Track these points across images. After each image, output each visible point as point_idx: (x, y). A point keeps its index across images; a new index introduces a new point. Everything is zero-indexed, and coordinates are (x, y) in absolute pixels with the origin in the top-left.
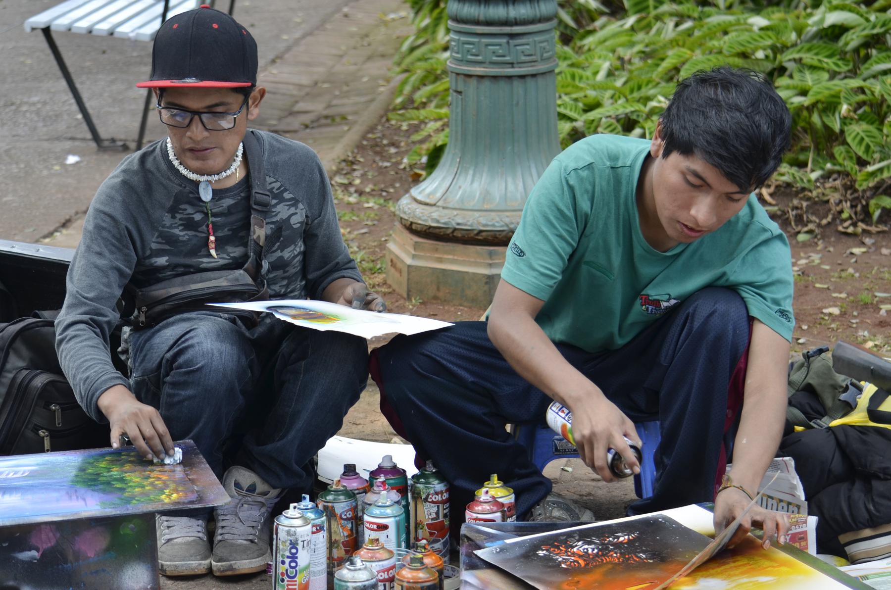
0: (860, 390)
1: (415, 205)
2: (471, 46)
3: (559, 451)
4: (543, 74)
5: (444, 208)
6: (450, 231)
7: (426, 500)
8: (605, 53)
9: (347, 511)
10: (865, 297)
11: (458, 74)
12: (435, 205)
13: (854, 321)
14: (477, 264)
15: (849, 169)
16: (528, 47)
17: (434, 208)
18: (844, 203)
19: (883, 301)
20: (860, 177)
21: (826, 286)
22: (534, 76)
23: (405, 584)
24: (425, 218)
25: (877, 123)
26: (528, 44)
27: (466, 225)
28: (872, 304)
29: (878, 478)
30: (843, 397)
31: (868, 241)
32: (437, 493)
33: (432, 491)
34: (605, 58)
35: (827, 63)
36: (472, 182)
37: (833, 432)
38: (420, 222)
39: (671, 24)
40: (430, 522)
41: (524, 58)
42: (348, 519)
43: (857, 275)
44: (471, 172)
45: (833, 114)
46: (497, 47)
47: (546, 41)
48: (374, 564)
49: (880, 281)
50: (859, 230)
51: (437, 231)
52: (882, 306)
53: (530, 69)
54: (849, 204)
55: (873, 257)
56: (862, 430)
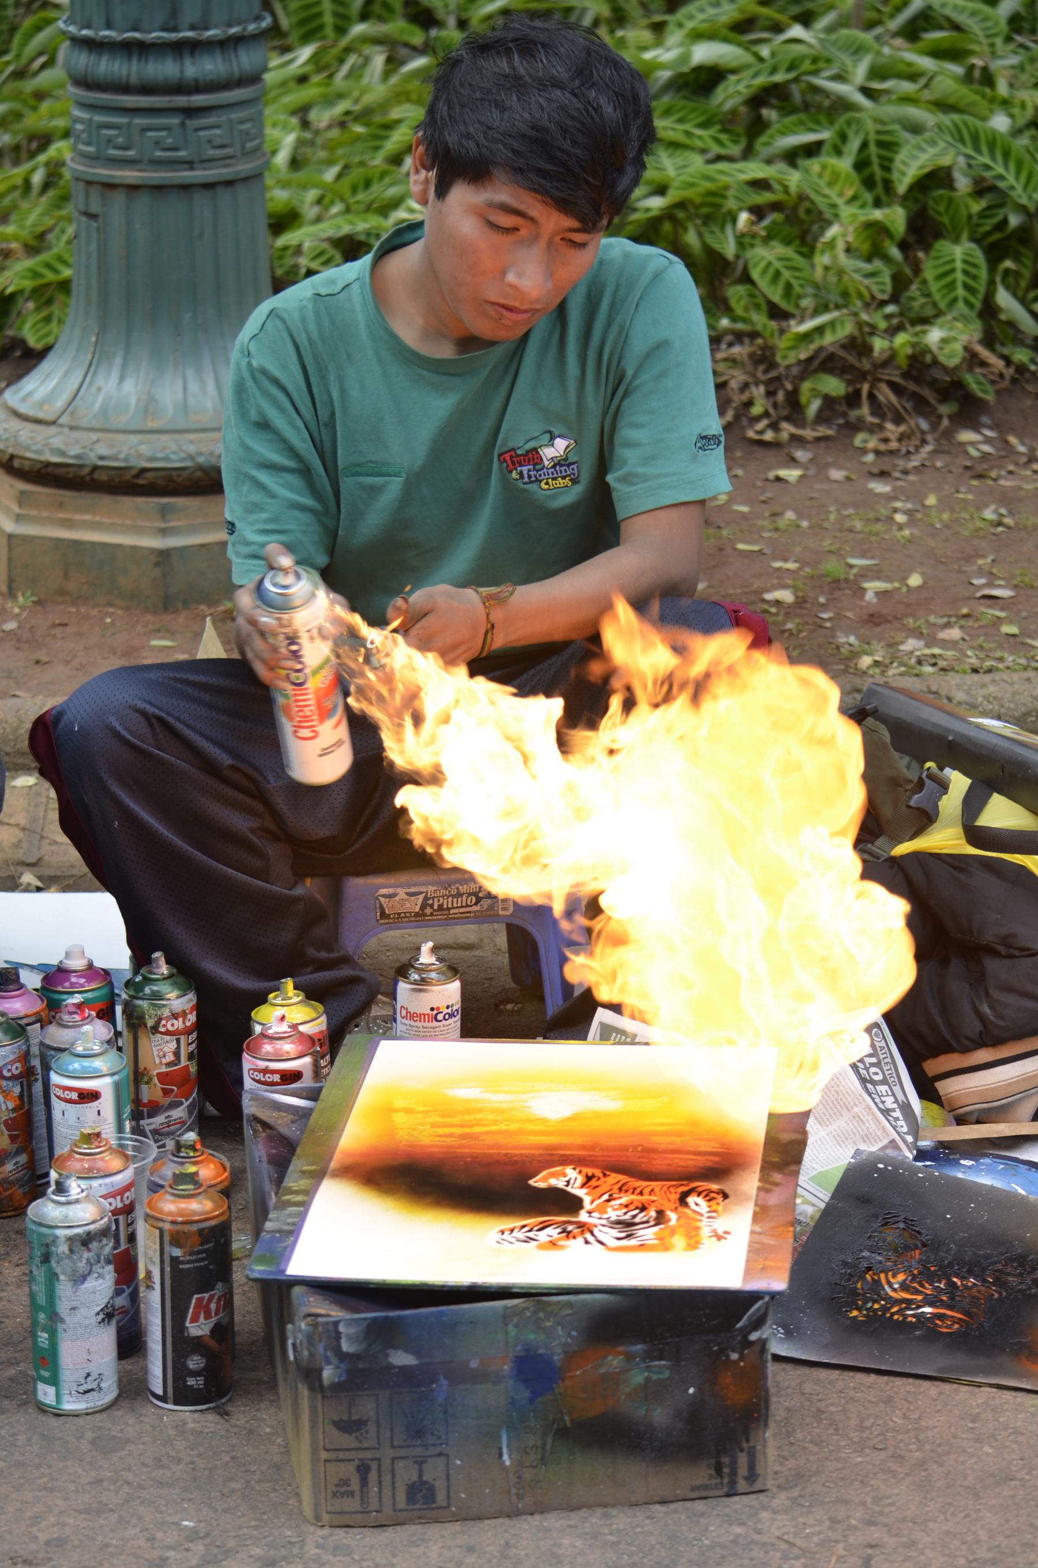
0: (944, 787)
1: (15, 424)
2: (114, 132)
3: (388, 917)
4: (246, 179)
5: (72, 428)
6: (87, 470)
7: (155, 1029)
8: (282, 117)
9: (12, 1063)
10: (832, 567)
11: (89, 183)
12: (53, 423)
13: (825, 616)
14: (139, 530)
15: (759, 327)
16: (218, 131)
17: (53, 430)
18: (753, 389)
19: (866, 574)
20: (782, 343)
21: (756, 548)
22: (229, 183)
23: (167, 1226)
24: (38, 447)
25: (797, 242)
26: (218, 127)
27: (116, 459)
28: (847, 580)
29: (997, 954)
30: (915, 800)
31: (800, 454)
32: (175, 1016)
33: (166, 1013)
34: (286, 128)
35: (700, 137)
36: (122, 379)
37: (901, 868)
38: (29, 455)
39: (379, 61)
40: (164, 1069)
41: (211, 152)
42: (14, 1078)
43: (805, 524)
44: (118, 361)
45: (722, 228)
46: (164, 133)
47: (250, 119)
48: (95, 1183)
49: (851, 536)
50: (784, 436)
51: (62, 471)
52: (866, 585)
53: (224, 171)
54: (762, 389)
55: (818, 486)
56: (955, 862)
